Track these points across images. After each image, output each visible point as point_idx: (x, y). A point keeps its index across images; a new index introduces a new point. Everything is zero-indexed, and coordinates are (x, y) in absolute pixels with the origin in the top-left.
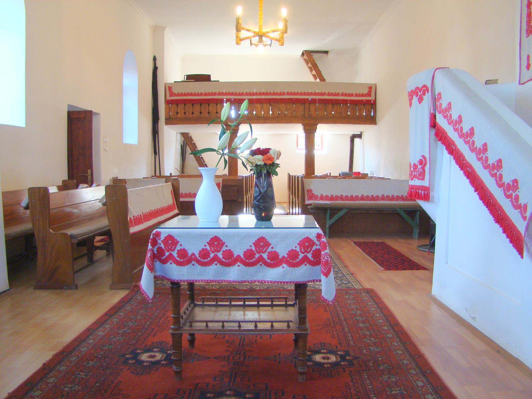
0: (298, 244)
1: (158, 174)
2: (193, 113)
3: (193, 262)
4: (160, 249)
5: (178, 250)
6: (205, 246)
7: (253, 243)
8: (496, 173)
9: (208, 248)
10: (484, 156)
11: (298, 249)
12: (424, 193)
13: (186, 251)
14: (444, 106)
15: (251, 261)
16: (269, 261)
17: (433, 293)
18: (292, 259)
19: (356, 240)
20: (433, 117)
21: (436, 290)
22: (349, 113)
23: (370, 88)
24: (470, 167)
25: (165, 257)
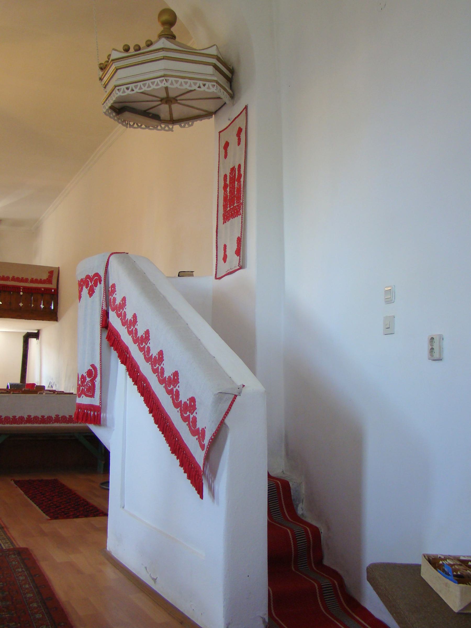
8: (172, 389)
10: (160, 368)
12: (94, 414)
14: (118, 302)
17: (108, 549)
19: (17, 479)
20: (105, 315)
21: (112, 545)
22: (21, 304)
24: (145, 380)
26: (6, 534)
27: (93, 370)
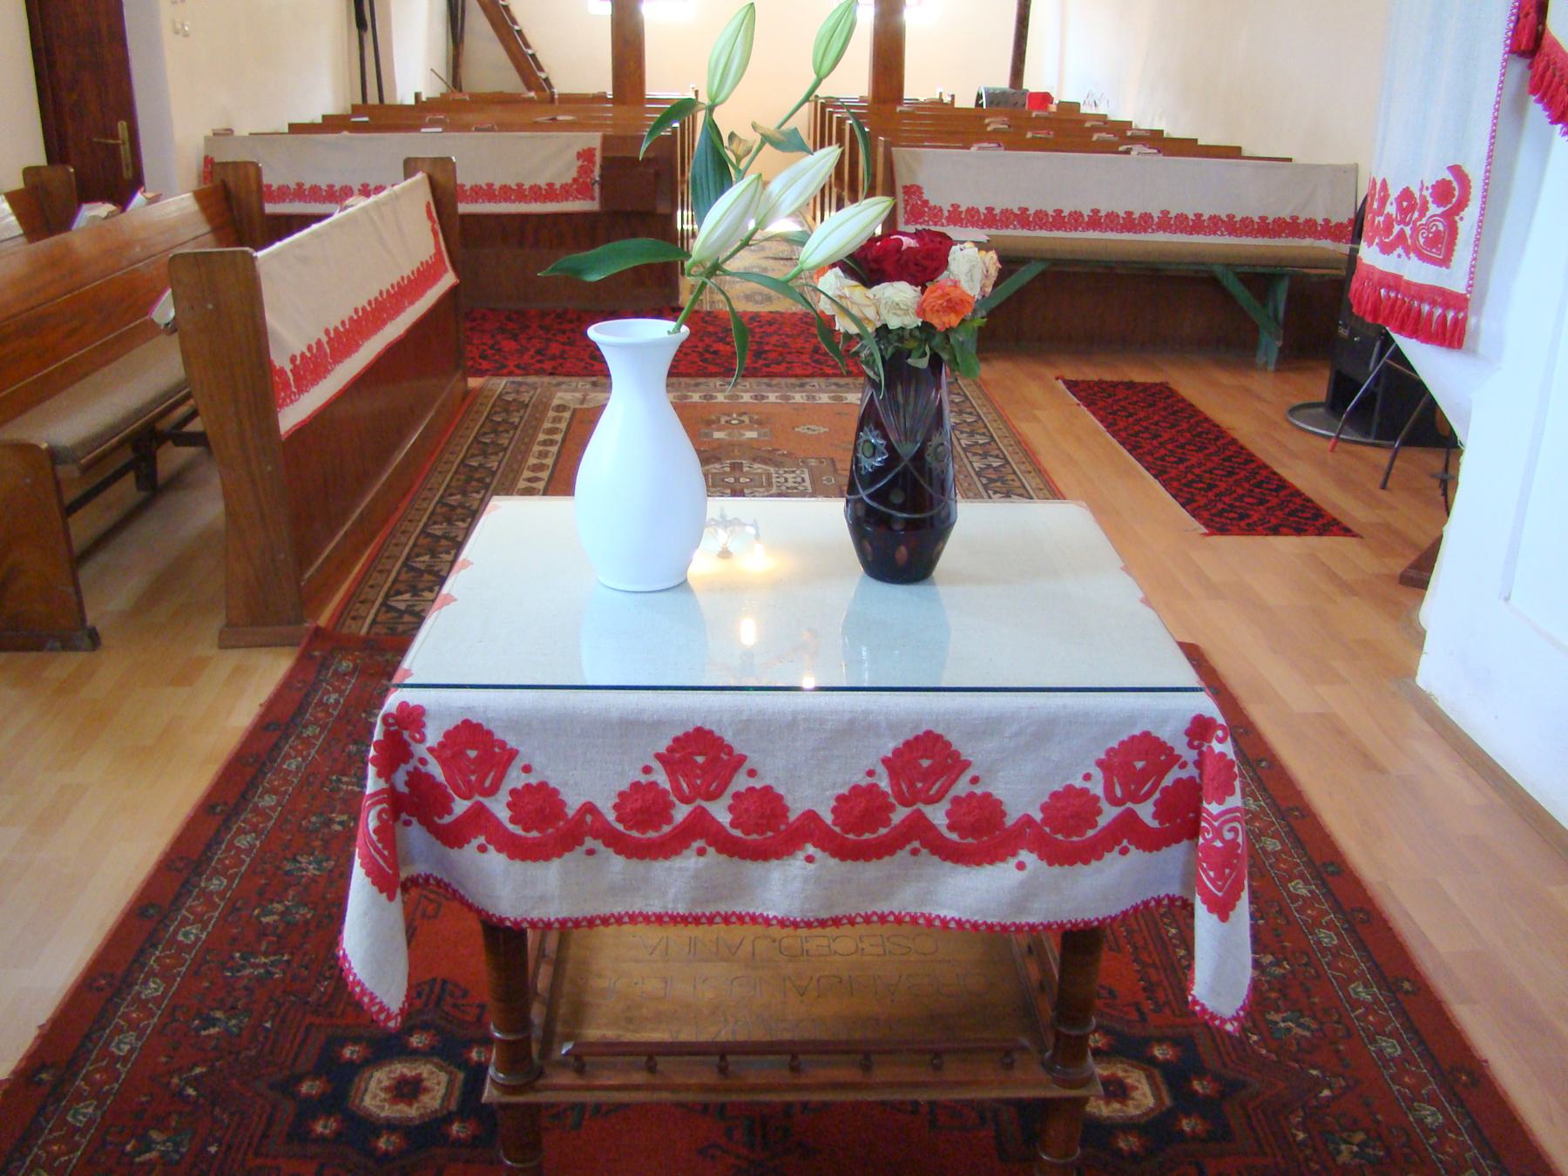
0: (1100, 763)
1: (373, 99)
3: (589, 842)
4: (419, 779)
5: (513, 792)
6: (647, 770)
7: (885, 761)
9: (661, 778)
11: (1097, 788)
12: (1444, 317)
13: (555, 792)
15: (867, 836)
16: (954, 836)
17: (1420, 681)
18: (1066, 832)
19: (1072, 375)
21: (1434, 673)
25: (447, 819)
27: (1455, 184)
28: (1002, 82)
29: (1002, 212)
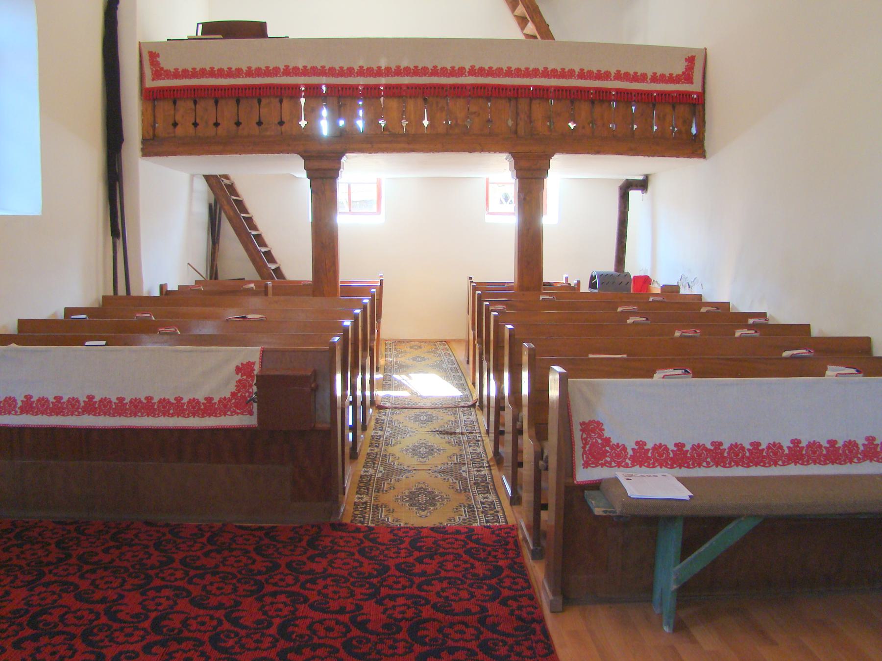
1: (122, 292)
2: (217, 124)
23: (691, 60)
26: (409, 471)
28: (609, 267)
29: (693, 448)
